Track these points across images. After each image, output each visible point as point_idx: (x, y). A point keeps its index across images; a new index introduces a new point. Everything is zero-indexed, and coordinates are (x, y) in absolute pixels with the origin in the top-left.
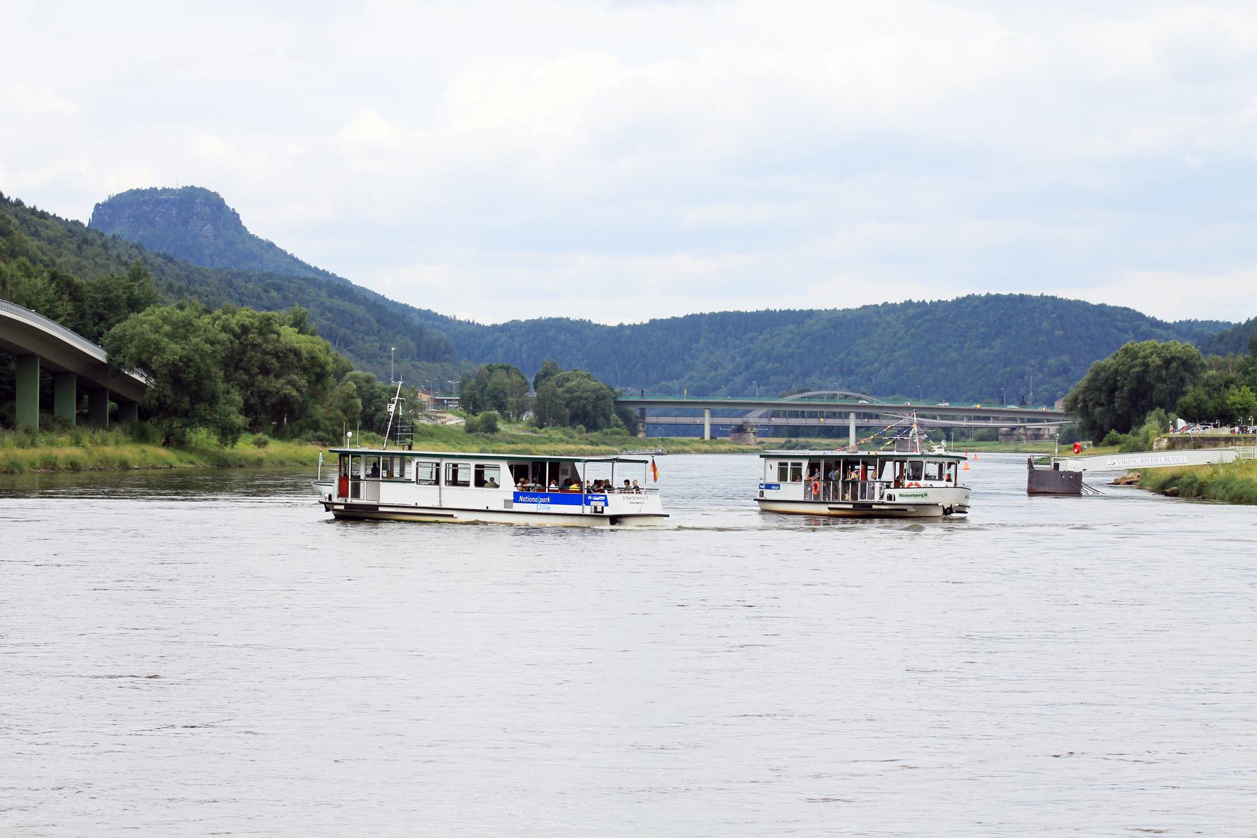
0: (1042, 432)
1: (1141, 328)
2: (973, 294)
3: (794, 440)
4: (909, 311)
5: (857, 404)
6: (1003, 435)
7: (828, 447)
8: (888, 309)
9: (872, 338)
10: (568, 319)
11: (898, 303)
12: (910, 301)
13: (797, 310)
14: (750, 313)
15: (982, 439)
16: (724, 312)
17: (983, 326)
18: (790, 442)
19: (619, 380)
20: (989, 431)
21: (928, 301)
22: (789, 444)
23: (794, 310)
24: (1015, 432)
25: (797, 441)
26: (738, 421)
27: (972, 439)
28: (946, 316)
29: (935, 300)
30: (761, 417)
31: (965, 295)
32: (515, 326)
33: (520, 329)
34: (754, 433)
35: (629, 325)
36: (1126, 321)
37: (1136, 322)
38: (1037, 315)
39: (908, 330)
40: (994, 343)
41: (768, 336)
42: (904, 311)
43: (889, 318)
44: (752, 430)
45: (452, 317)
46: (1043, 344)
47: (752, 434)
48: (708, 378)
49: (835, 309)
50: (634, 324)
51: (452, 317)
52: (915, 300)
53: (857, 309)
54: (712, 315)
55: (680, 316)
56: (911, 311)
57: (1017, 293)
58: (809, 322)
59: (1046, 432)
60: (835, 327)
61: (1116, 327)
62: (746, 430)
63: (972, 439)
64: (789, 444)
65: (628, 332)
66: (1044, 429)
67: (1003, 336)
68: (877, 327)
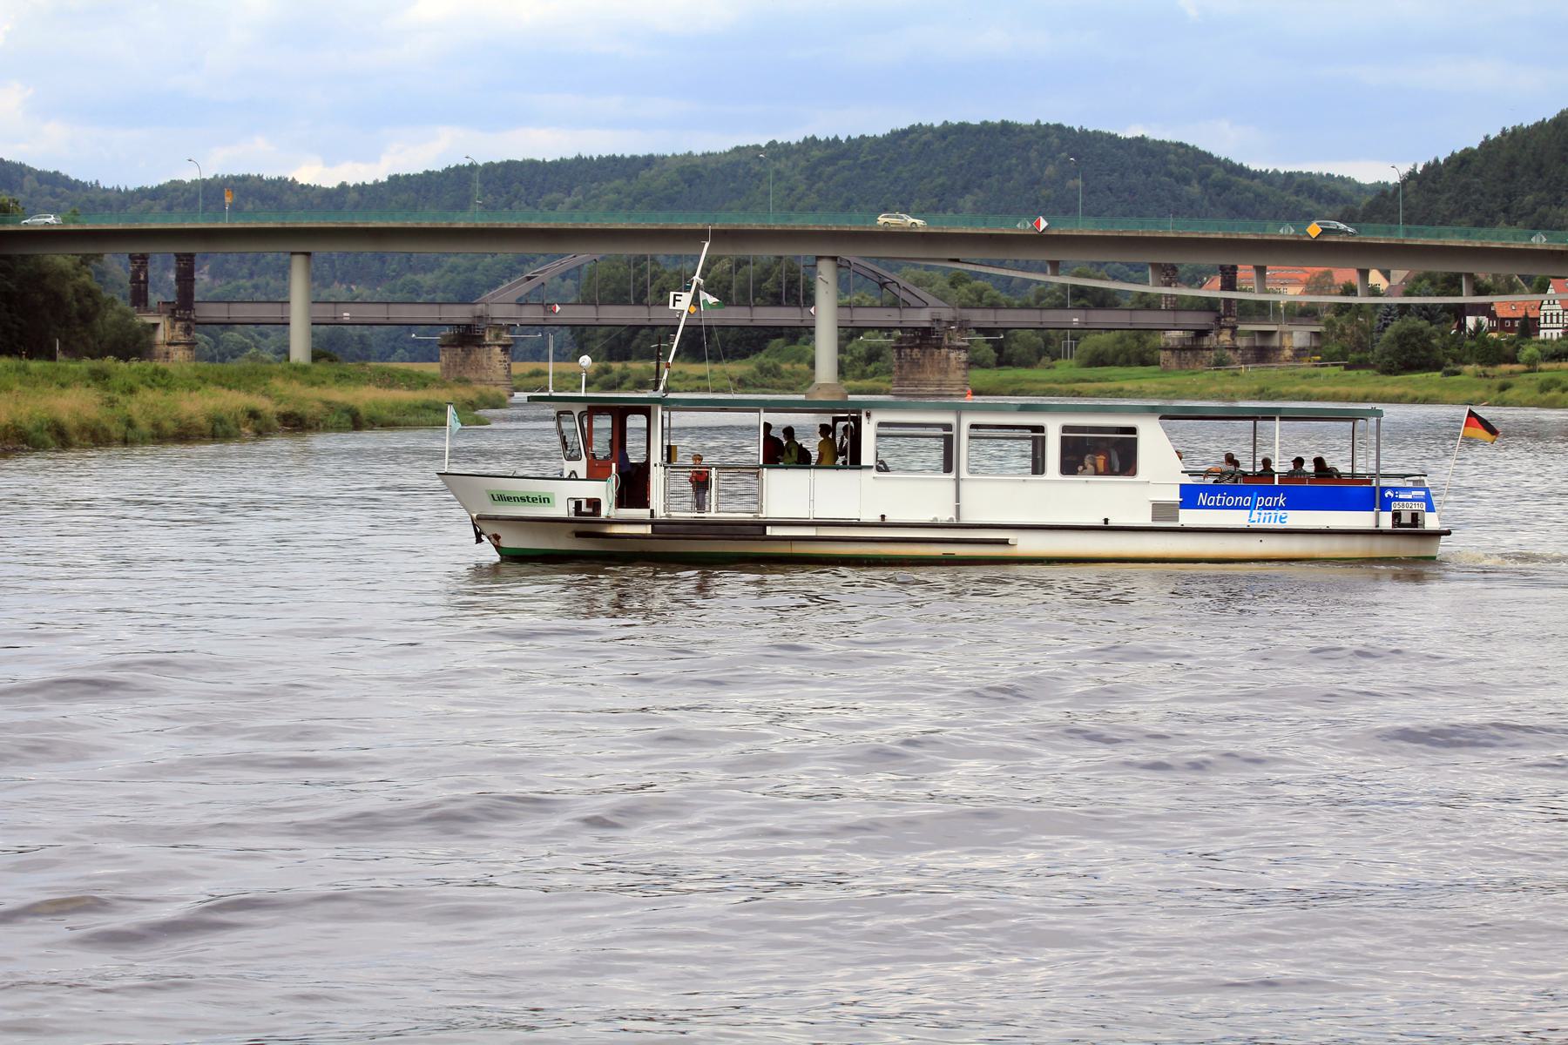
0: (1275, 342)
1: (1213, 176)
2: (920, 124)
3: (617, 366)
4: (813, 153)
5: (868, 227)
6: (1173, 349)
7: (702, 384)
8: (777, 151)
9: (751, 199)
10: (260, 178)
11: (793, 142)
12: (814, 138)
13: (627, 155)
14: (551, 163)
15: (1098, 360)
16: (509, 161)
17: (940, 174)
18: (607, 371)
19: (338, 274)
20: (1121, 340)
21: (843, 138)
22: (605, 377)
23: (622, 156)
24: (1206, 342)
25: (625, 368)
26: (461, 314)
27: (1073, 362)
28: (877, 160)
29: (855, 136)
30: (521, 303)
31: (905, 126)
32: (175, 190)
33: (183, 194)
34: (505, 348)
35: (356, 186)
36: (1185, 164)
37: (1202, 166)
38: (1033, 154)
39: (814, 184)
40: (960, 202)
41: (580, 197)
42: (804, 154)
43: (778, 165)
44: (497, 337)
45: (94, 183)
46: (1047, 201)
47: (498, 350)
48: (479, 268)
49: (690, 153)
50: (364, 183)
51: (94, 183)
52: (821, 137)
53: (725, 154)
54: (490, 168)
55: (436, 170)
56: (816, 153)
57: (995, 119)
58: (645, 174)
59: (1286, 342)
60: (690, 183)
61: (1170, 174)
62: (482, 337)
63: (1073, 362)
64: (605, 377)
65: (355, 196)
66: (1282, 333)
67: (976, 190)
68: (760, 181)
